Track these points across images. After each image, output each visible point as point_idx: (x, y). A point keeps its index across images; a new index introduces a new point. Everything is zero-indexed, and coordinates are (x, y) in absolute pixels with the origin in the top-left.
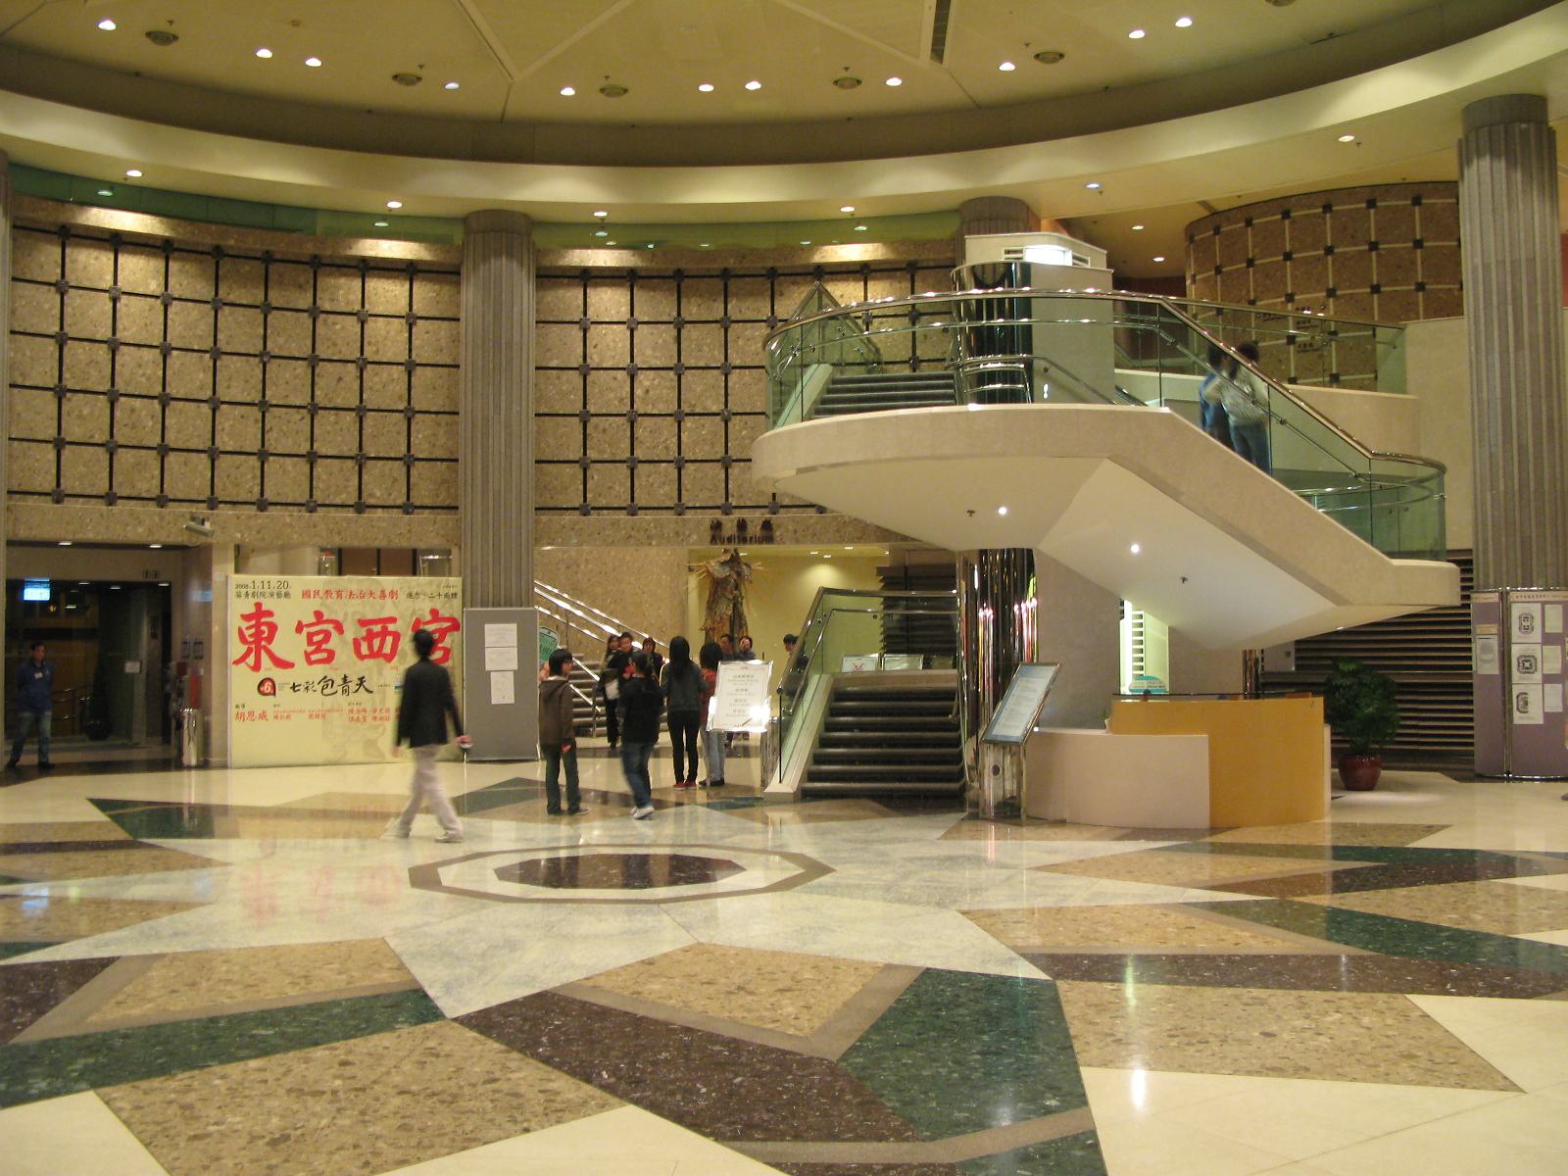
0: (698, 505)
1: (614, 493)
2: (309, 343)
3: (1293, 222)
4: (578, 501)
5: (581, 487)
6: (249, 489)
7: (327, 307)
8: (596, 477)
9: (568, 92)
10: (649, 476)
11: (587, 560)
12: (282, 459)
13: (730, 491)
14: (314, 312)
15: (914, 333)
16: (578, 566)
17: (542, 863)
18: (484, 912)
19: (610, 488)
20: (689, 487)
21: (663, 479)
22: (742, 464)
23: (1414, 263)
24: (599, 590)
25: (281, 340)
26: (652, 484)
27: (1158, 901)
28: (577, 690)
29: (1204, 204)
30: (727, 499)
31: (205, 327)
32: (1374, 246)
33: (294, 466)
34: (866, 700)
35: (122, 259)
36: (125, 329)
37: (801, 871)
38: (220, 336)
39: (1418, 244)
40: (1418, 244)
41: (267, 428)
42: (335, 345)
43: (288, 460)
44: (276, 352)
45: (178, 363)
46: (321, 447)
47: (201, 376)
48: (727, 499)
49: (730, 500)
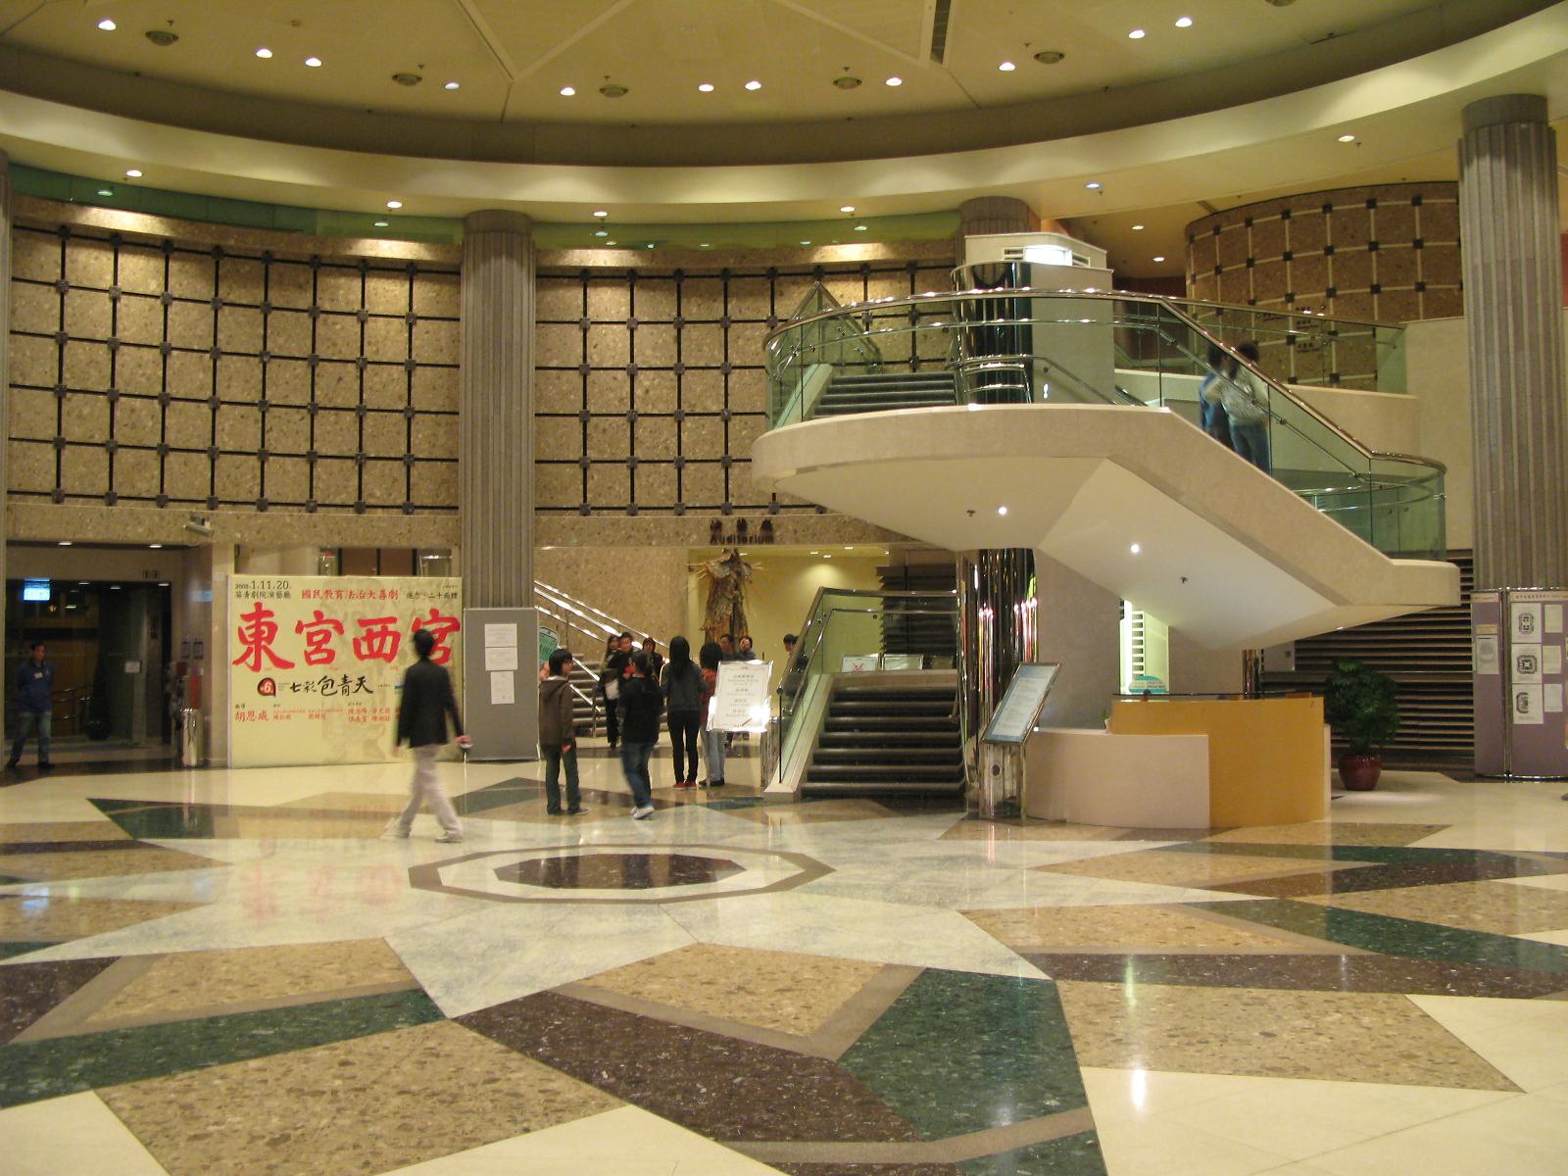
0: (698, 505)
1: (614, 493)
2: (309, 343)
3: (1293, 222)
4: (578, 501)
5: (581, 487)
6: (249, 489)
7: (327, 307)
8: (596, 477)
9: (568, 92)
10: (649, 476)
11: (587, 560)
12: (282, 459)
13: (730, 491)
14: (314, 312)
15: (914, 333)
16: (578, 566)
17: (542, 863)
18: (484, 912)
19: (610, 488)
20: (689, 487)
21: (663, 479)
22: (742, 464)
23: (1414, 263)
24: (599, 590)
25: (281, 340)
26: (652, 484)
27: (1158, 901)
28: (577, 690)
29: (1204, 204)
30: (727, 499)
31: (205, 327)
32: (1374, 246)
33: (294, 466)
34: (866, 700)
35: (122, 259)
36: (125, 329)
37: (801, 871)
38: (220, 336)
39: (1418, 244)
40: (1418, 244)
41: (267, 428)
42: (335, 345)
43: (288, 460)
44: (276, 352)
45: (178, 363)
46: (321, 447)
47: (201, 376)
48: (727, 499)
49: (730, 500)
